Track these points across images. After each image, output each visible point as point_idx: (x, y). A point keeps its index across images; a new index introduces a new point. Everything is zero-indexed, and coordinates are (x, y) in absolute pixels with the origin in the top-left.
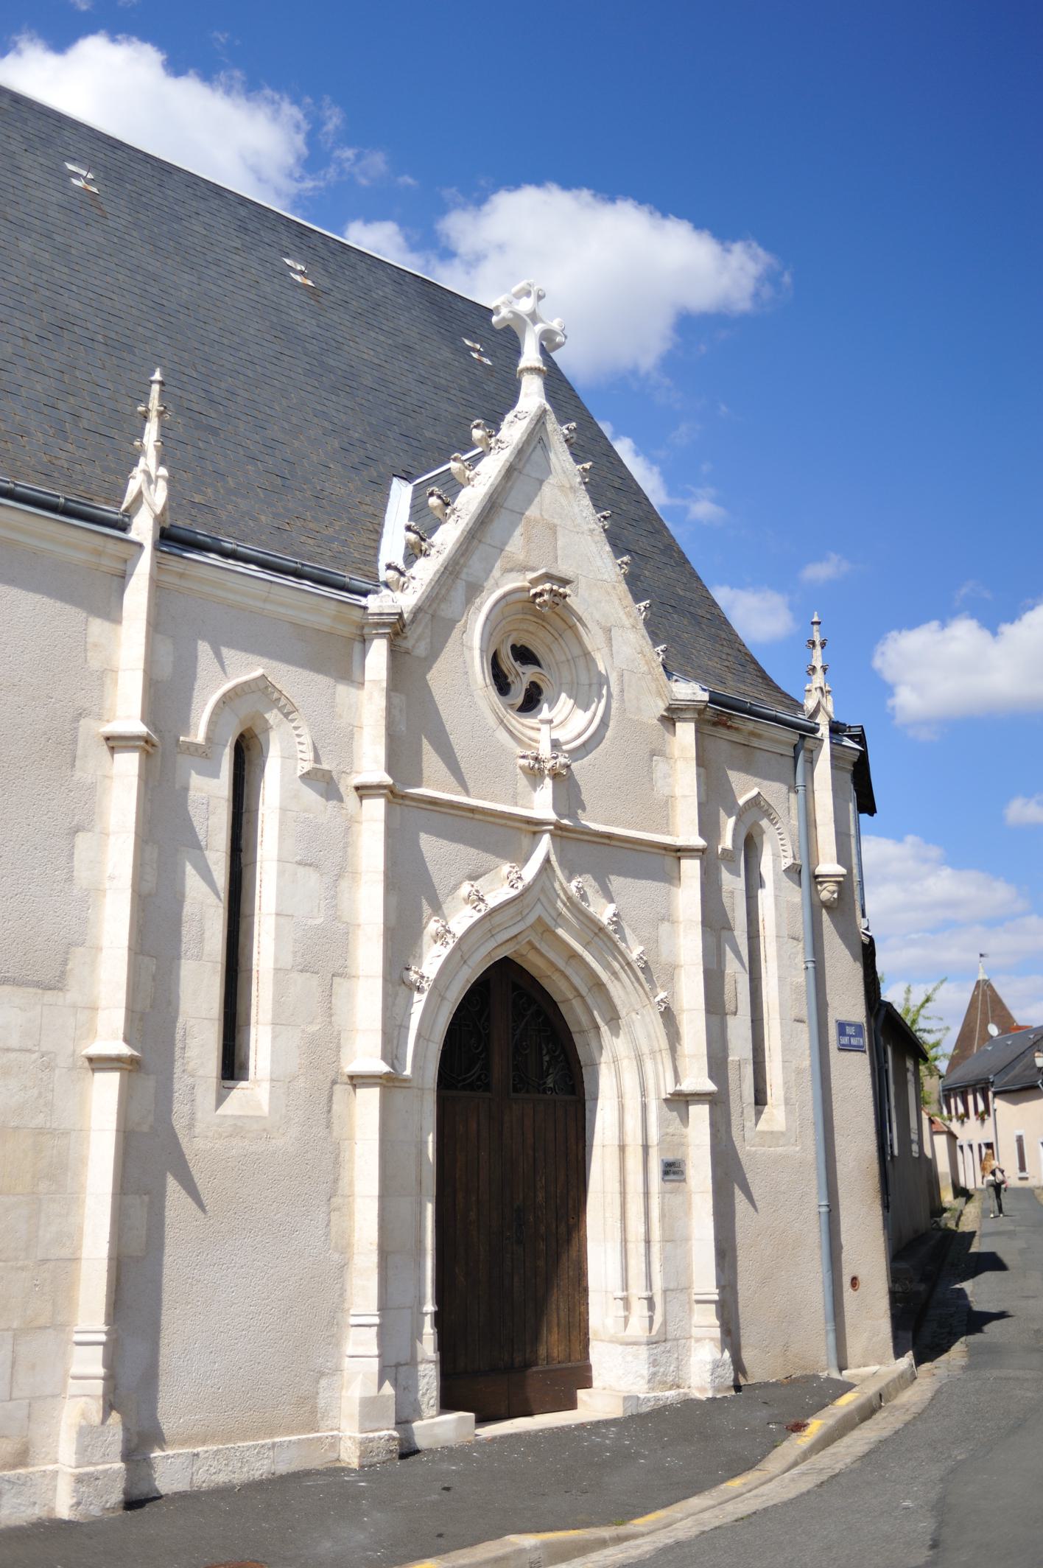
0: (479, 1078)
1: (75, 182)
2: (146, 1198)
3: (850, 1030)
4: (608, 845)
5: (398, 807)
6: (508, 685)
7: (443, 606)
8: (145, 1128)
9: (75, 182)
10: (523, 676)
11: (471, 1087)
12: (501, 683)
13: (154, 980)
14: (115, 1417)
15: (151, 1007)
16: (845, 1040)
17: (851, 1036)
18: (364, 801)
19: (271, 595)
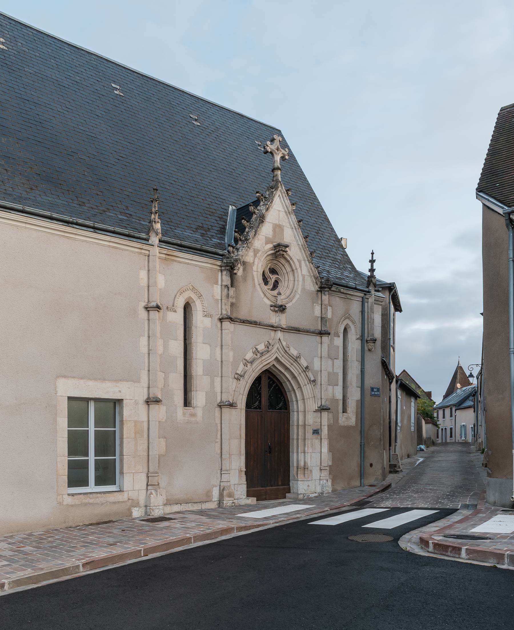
0: (258, 406)
1: (116, 92)
2: (165, 439)
3: (375, 390)
4: (299, 333)
5: (233, 324)
6: (268, 282)
7: (246, 258)
8: (164, 420)
9: (116, 92)
10: (273, 278)
11: (256, 408)
12: (266, 281)
13: (164, 379)
14: (363, 267)
15: (164, 387)
16: (373, 393)
17: (375, 392)
18: (223, 323)
19: (242, 395)
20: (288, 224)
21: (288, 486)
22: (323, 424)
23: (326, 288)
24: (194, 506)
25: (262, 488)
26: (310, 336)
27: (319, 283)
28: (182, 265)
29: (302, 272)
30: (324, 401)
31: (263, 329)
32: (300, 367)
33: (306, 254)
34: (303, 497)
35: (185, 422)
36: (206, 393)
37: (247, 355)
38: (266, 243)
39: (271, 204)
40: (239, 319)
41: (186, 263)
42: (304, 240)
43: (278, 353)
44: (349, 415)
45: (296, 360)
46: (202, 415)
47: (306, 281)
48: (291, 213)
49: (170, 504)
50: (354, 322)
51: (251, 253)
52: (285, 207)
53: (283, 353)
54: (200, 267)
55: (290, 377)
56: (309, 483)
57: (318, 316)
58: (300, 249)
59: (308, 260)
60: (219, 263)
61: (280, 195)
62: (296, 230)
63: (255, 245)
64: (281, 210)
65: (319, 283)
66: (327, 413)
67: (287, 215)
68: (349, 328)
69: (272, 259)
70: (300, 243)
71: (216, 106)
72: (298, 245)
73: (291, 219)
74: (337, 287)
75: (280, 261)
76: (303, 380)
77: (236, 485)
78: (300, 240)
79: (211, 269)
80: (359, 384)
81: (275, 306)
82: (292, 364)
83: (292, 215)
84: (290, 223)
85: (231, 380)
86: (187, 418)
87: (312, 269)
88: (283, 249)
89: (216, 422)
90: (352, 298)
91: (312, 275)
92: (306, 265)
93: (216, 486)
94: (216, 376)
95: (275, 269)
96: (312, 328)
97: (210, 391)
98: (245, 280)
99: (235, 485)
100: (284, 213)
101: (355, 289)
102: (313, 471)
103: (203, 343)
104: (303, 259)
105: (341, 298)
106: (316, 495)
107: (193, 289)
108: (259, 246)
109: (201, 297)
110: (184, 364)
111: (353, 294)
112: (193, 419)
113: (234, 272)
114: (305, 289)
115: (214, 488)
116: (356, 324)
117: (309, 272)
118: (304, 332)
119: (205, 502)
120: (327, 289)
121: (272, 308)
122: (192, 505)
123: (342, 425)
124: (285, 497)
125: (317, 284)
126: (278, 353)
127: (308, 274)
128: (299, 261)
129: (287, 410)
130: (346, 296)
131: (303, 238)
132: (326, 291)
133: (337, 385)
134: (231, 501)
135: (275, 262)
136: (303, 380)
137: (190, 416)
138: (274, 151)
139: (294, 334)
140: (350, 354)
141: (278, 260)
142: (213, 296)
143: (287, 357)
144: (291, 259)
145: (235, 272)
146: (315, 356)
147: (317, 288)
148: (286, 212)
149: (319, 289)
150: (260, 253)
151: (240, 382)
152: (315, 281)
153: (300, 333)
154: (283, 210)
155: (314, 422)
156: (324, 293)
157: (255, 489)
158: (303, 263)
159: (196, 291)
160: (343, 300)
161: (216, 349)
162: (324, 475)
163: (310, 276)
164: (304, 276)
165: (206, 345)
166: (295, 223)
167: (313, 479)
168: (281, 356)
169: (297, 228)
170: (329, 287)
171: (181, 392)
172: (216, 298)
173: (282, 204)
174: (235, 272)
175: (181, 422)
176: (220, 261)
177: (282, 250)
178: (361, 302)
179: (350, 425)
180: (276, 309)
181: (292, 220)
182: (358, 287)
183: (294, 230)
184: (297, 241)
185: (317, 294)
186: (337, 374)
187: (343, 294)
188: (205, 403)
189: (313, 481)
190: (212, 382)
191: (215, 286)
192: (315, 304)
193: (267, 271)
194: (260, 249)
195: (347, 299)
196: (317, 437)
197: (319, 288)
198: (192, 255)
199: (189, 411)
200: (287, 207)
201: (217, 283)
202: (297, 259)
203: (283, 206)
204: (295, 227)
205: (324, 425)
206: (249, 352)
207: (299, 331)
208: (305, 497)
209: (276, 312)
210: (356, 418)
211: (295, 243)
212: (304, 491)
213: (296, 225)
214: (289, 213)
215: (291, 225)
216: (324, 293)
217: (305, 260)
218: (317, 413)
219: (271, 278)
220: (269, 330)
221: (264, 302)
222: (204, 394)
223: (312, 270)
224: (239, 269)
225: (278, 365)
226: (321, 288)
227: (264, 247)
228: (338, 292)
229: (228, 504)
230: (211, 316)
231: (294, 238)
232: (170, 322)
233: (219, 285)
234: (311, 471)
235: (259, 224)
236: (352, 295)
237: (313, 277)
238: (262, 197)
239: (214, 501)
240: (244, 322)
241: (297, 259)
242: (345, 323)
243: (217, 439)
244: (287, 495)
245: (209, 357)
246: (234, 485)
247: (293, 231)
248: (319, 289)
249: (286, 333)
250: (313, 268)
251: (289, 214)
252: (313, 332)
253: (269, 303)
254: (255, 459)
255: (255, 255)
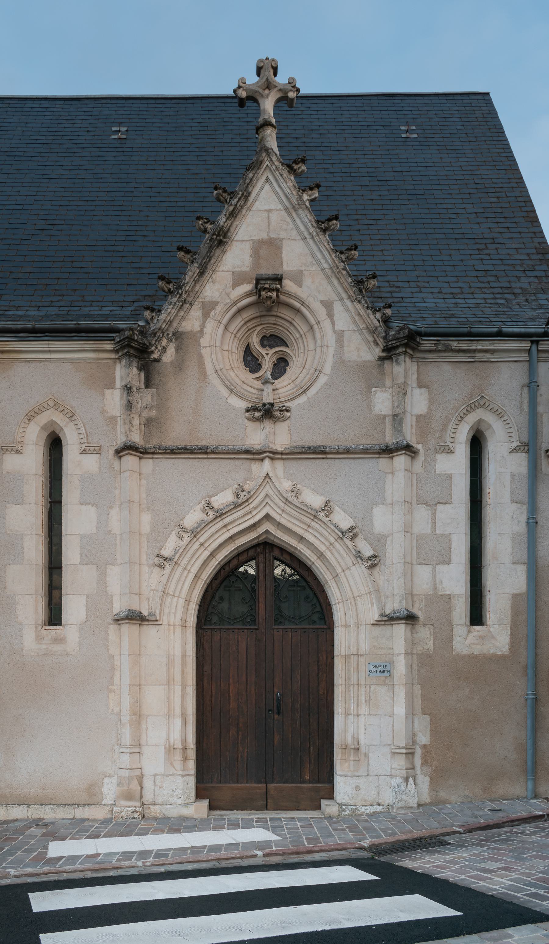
4: (326, 458)
5: (151, 460)
7: (184, 324)
20: (295, 233)
21: (327, 785)
22: (397, 652)
23: (397, 347)
24: (58, 810)
25: (256, 785)
26: (360, 460)
27: (381, 342)
28: (33, 365)
29: (334, 327)
30: (398, 601)
31: (227, 461)
32: (329, 531)
33: (342, 284)
34: (340, 812)
35: (40, 654)
36: (87, 597)
37: (187, 517)
38: (235, 285)
39: (242, 202)
40: (159, 448)
41: (40, 361)
42: (334, 255)
43: (272, 505)
44: (492, 629)
45: (315, 517)
46: (77, 640)
47: (346, 343)
48: (297, 207)
49: (6, 805)
50: (499, 414)
51: (196, 313)
52: (284, 198)
53: (283, 504)
54: (72, 362)
55: (313, 555)
56: (361, 782)
57: (383, 413)
58: (328, 277)
59: (350, 297)
60: (109, 346)
61: (271, 177)
62: (314, 241)
63: (206, 294)
64: (273, 207)
65: (381, 340)
66: (403, 626)
67: (289, 214)
68: (488, 429)
69: (258, 314)
70: (326, 266)
71: (348, 98)
72: (323, 270)
73: (300, 219)
74: (438, 340)
75: (279, 314)
76: (342, 557)
77: (160, 777)
78: (325, 258)
79: (97, 361)
80: (523, 555)
81: (255, 409)
82: (309, 526)
83: (300, 211)
84: (297, 229)
85: (145, 569)
86: (44, 647)
87: (359, 314)
88: (267, 286)
89: (110, 652)
90: (493, 358)
91: (362, 326)
92: (347, 310)
93: (110, 776)
94: (111, 564)
95: (279, 336)
96: (365, 443)
97: (97, 592)
98: (181, 369)
99: (157, 777)
100: (284, 213)
101: (500, 334)
102: (371, 755)
103: (81, 504)
104: (337, 298)
105: (458, 364)
106: (379, 808)
107: (57, 406)
108: (217, 294)
109: (73, 419)
110: (60, 545)
111: (492, 347)
112: (57, 648)
113: (152, 357)
114: (343, 361)
115: (106, 780)
116: (506, 418)
117: (355, 322)
118: (338, 453)
119: (84, 805)
120: (401, 350)
121: (248, 414)
122: (52, 809)
123: (465, 653)
124: (318, 808)
125: (376, 343)
126: (272, 505)
127: (352, 327)
128: (328, 306)
129: (255, 625)
130: (473, 357)
131: (331, 253)
132: (399, 355)
133: (448, 563)
134: (132, 808)
135: (271, 320)
136: (342, 557)
137: (51, 642)
138: (257, 92)
139: (313, 461)
140: (491, 488)
141: (275, 313)
142: (103, 411)
143: (298, 514)
144: (303, 303)
145: (155, 356)
146: (377, 504)
147: (378, 352)
148: (286, 209)
149: (384, 355)
150: (219, 309)
151: (164, 572)
152: (371, 339)
153: (328, 456)
154: (280, 207)
155: (375, 647)
156: (397, 361)
157: (239, 785)
158: (338, 307)
159: (61, 409)
160: (465, 367)
161: (110, 512)
162: (399, 767)
163: (358, 330)
164: (340, 336)
165: (87, 506)
166: (310, 225)
167: (371, 773)
168: (280, 512)
169: (315, 234)
170: (403, 343)
171: (32, 597)
172: (109, 415)
173: (276, 193)
174: (155, 356)
175: (33, 654)
176: (108, 342)
177: (265, 289)
178: (526, 365)
179: (491, 652)
180: (257, 414)
181: (302, 222)
182: (505, 330)
183: (311, 242)
184: (319, 263)
185: (380, 365)
186: (448, 538)
187: (461, 355)
188: (85, 617)
189: (370, 778)
190: (102, 577)
191: (108, 392)
192: (373, 389)
193: (255, 342)
194: (218, 300)
195: (476, 365)
196: (384, 681)
197: (383, 351)
198: (47, 342)
199: (53, 633)
200: (287, 197)
201: (112, 386)
202: (322, 302)
203: (279, 198)
204: (310, 234)
205: (398, 655)
206: (192, 511)
207: (323, 452)
208: (344, 810)
209: (258, 420)
210: (513, 635)
211: (315, 268)
212: (346, 798)
213: (312, 230)
214: (294, 207)
215: (300, 233)
216: (397, 361)
217: (341, 299)
218: (384, 627)
219: (263, 356)
220: (244, 461)
221: (230, 405)
222: (83, 600)
223: (361, 316)
224: (164, 349)
225: (278, 532)
226: (386, 349)
227: (228, 295)
228: (445, 351)
229: (124, 814)
230: (98, 450)
231: (310, 259)
232: (8, 473)
233: (116, 389)
234: (367, 756)
235: (210, 249)
236: (493, 352)
237: (364, 331)
238: (224, 195)
239: (105, 805)
240: (172, 452)
241: (322, 302)
242: (472, 419)
243: (113, 684)
244: (324, 802)
245: (94, 528)
246: (155, 775)
247: (307, 245)
248: (384, 355)
249: (292, 461)
250: (362, 312)
251: (295, 210)
252: (365, 451)
253: (243, 405)
254: (241, 725)
255: (206, 315)
